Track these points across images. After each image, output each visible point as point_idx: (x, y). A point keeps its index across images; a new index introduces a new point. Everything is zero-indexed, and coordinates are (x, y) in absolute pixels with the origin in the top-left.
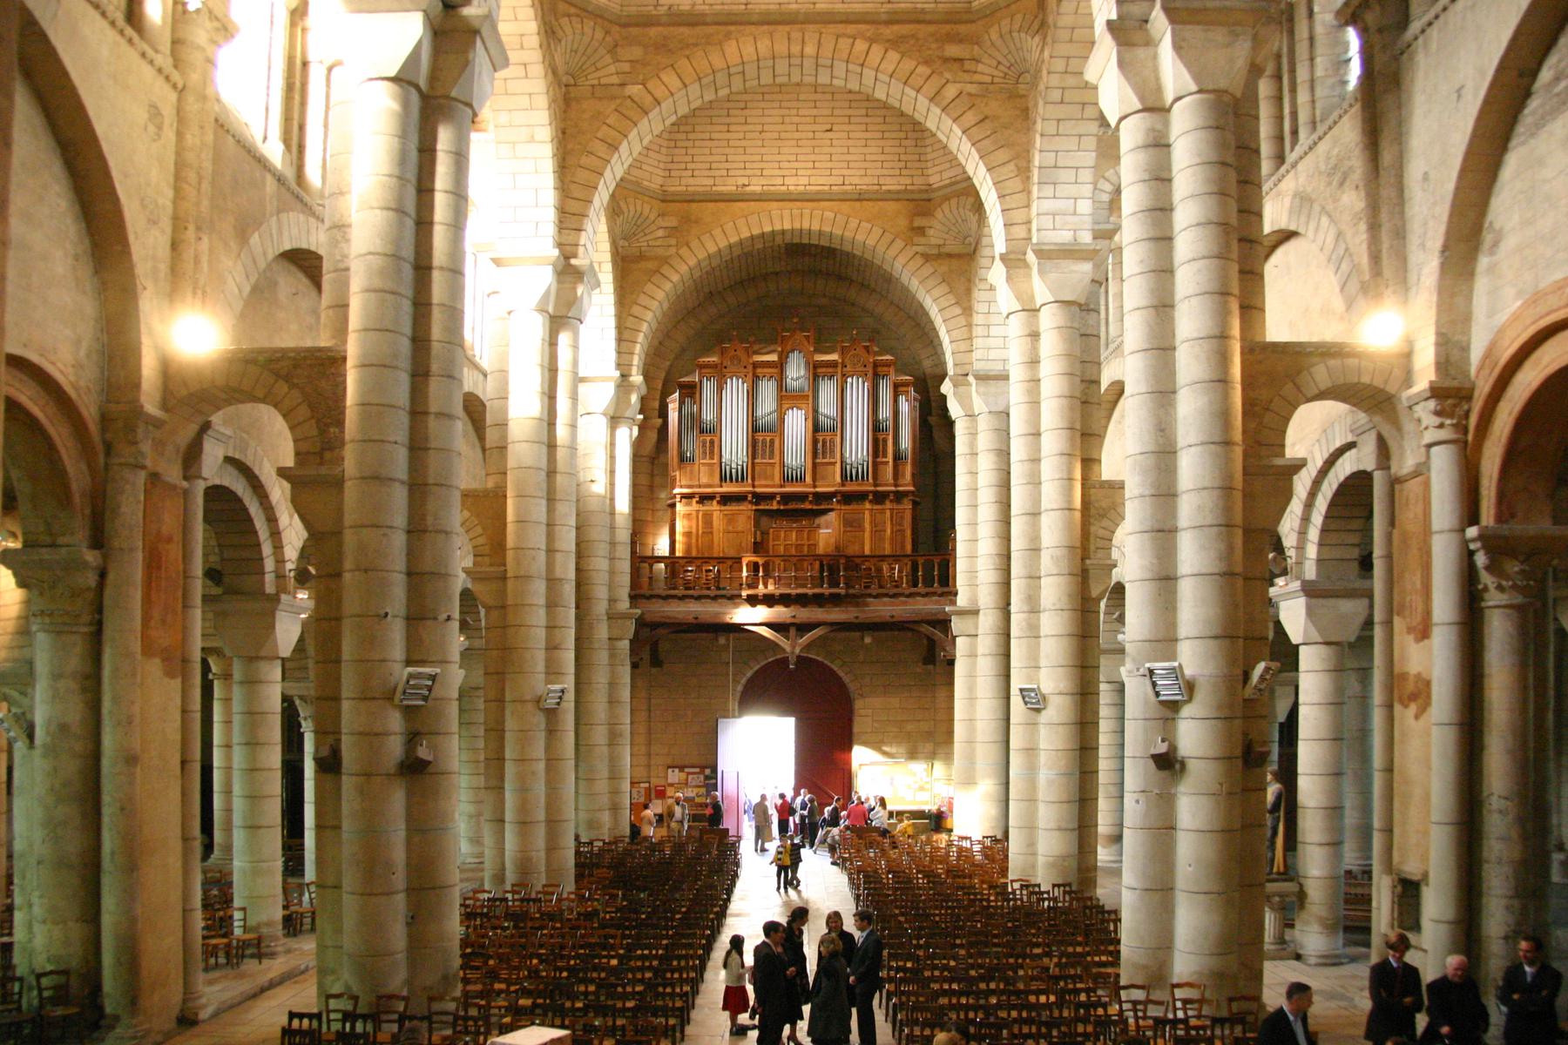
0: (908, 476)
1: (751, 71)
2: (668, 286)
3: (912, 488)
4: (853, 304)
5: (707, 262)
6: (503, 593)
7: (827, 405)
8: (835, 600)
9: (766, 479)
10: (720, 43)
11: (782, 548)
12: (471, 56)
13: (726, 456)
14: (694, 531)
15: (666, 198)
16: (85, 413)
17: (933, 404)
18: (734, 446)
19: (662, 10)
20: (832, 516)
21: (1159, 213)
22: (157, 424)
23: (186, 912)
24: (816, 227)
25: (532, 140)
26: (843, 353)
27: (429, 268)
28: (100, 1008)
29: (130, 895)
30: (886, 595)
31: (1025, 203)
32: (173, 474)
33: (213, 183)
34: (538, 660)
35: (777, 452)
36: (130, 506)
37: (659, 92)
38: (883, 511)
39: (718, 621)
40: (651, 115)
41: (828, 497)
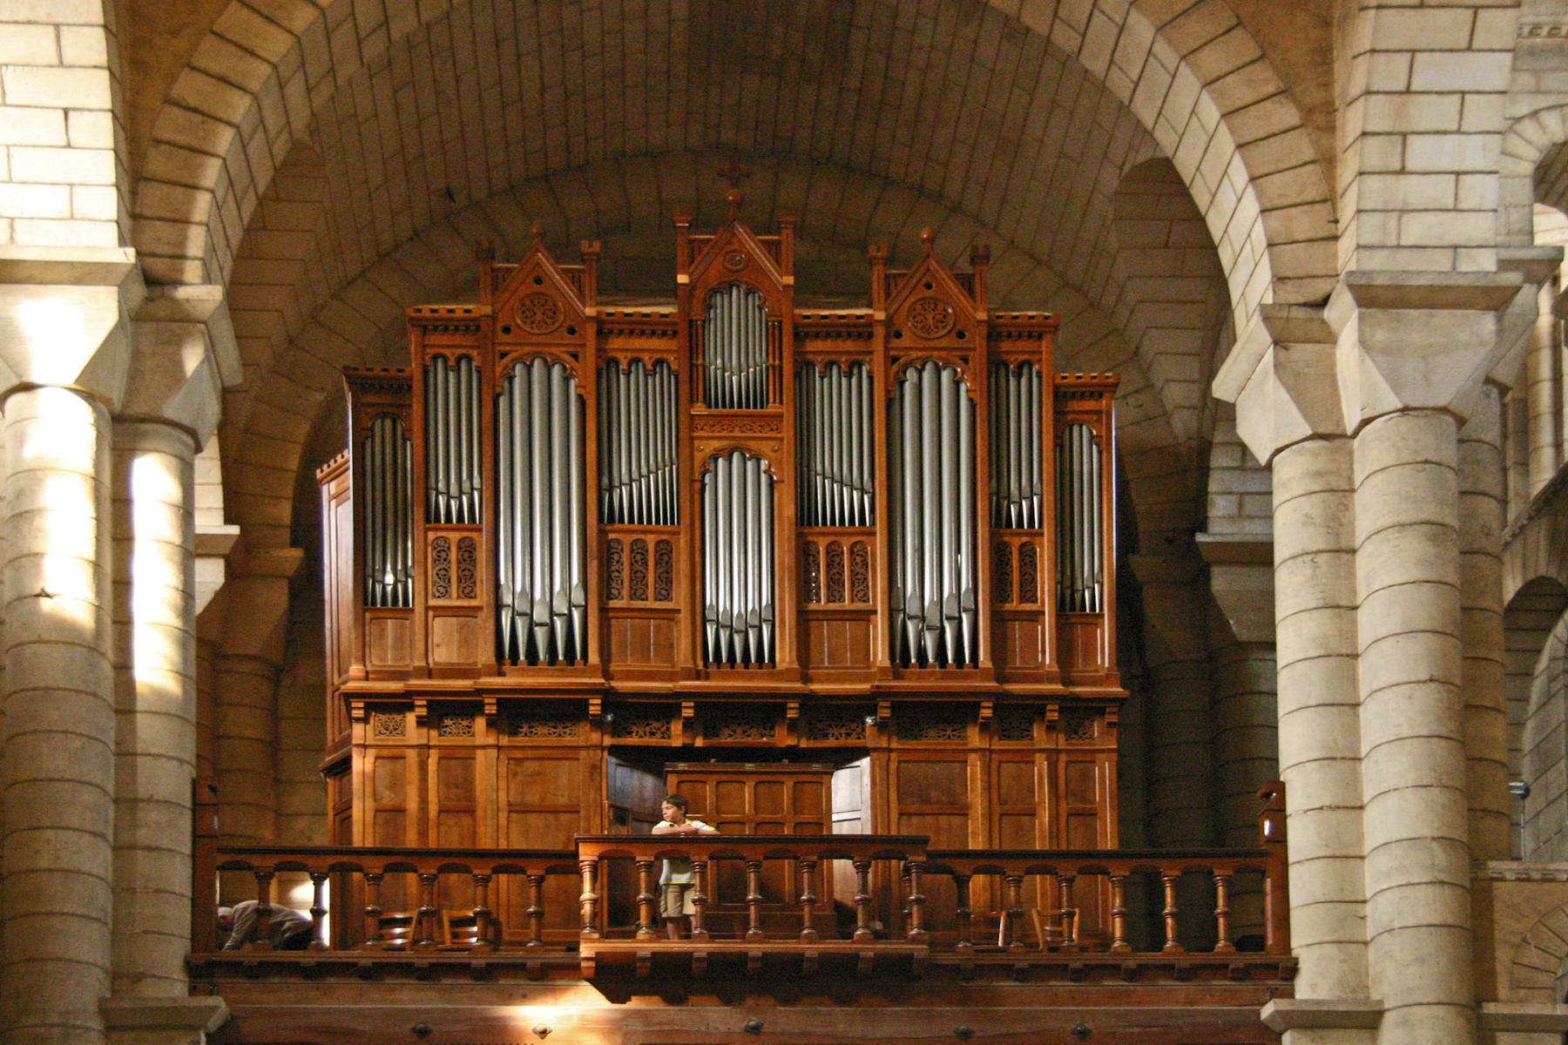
0: (1104, 657)
3: (1117, 690)
17: (1142, 526)
38: (1027, 757)
41: (848, 710)
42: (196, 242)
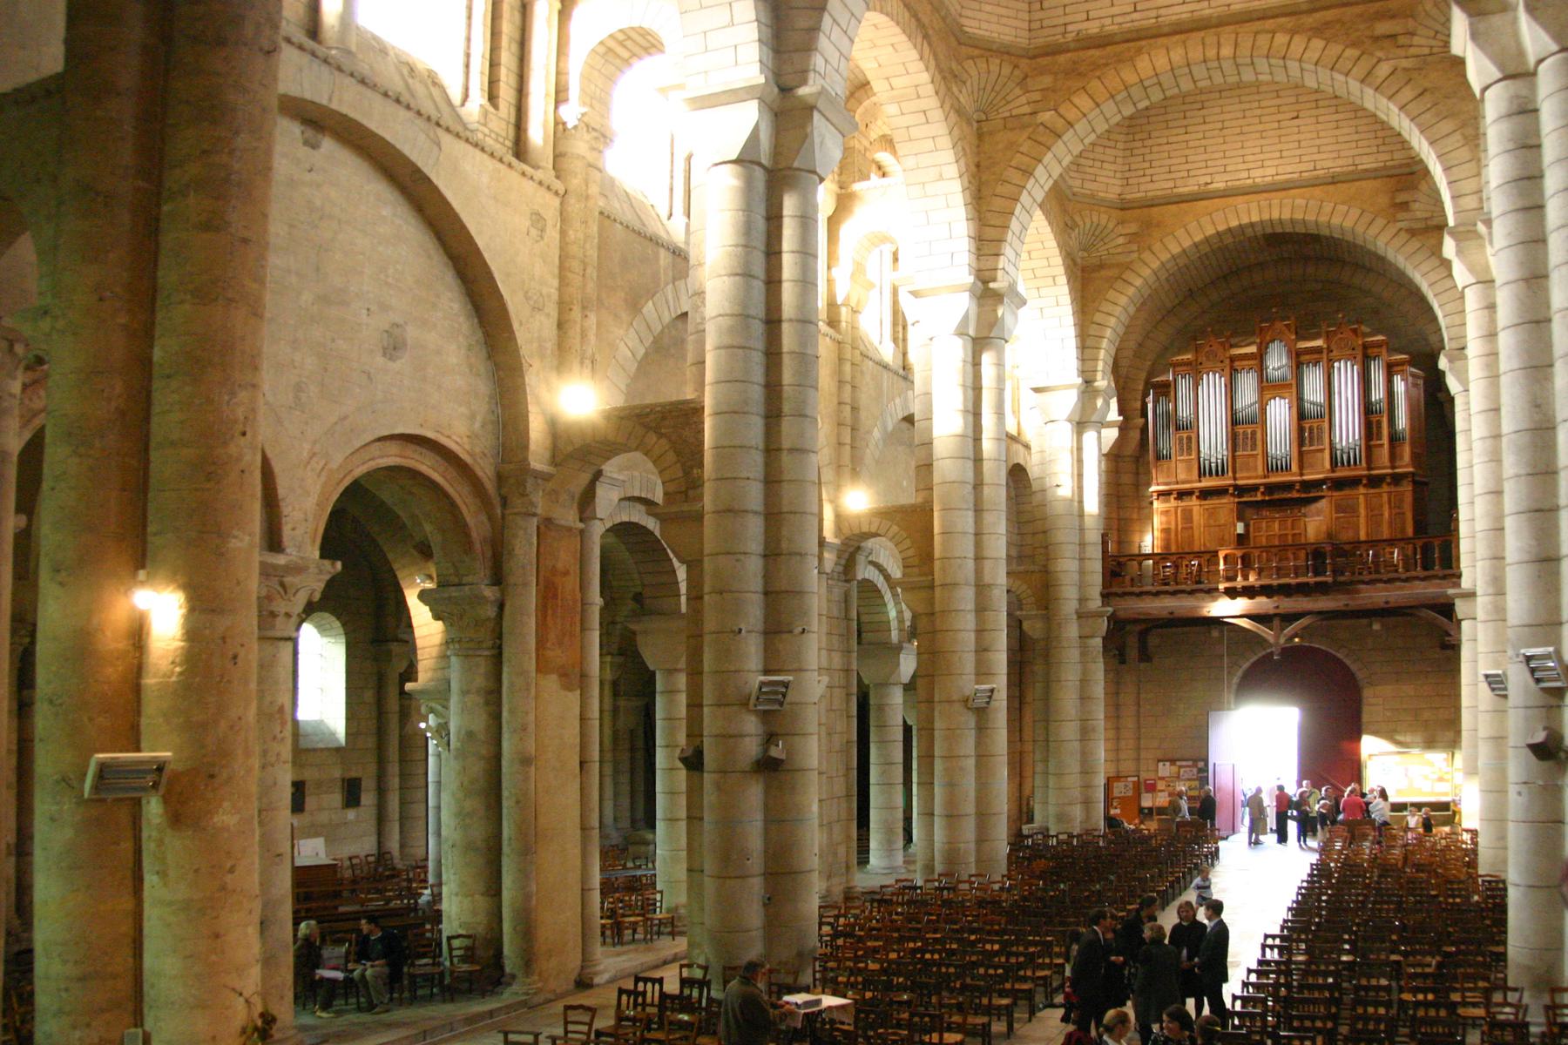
1: (1167, 80)
2: (1131, 291)
3: (1411, 469)
4: (1349, 286)
5: (1173, 263)
6: (931, 601)
7: (1313, 389)
8: (1322, 589)
9: (1248, 470)
10: (1132, 59)
11: (1264, 540)
12: (809, 130)
13: (1204, 450)
14: (1173, 527)
15: (1124, 206)
16: (480, 473)
18: (1213, 438)
19: (1070, 37)
20: (1323, 504)
21: (1526, 182)
22: (547, 477)
23: (585, 891)
24: (1286, 216)
25: (941, 178)
26: (1328, 339)
27: (780, 321)
28: (501, 968)
29: (524, 875)
30: (1380, 581)
31: (1474, 172)
32: (568, 516)
33: (599, 268)
34: (968, 662)
35: (1259, 443)
36: (524, 547)
37: (1071, 114)
39: (1196, 615)
40: (1065, 138)
41: (1317, 484)
42: (1100, 365)
